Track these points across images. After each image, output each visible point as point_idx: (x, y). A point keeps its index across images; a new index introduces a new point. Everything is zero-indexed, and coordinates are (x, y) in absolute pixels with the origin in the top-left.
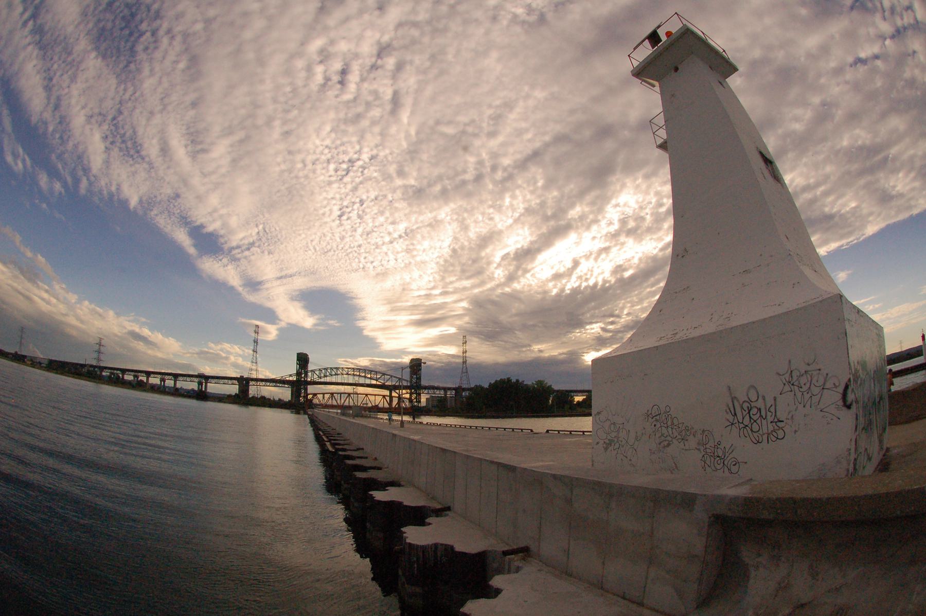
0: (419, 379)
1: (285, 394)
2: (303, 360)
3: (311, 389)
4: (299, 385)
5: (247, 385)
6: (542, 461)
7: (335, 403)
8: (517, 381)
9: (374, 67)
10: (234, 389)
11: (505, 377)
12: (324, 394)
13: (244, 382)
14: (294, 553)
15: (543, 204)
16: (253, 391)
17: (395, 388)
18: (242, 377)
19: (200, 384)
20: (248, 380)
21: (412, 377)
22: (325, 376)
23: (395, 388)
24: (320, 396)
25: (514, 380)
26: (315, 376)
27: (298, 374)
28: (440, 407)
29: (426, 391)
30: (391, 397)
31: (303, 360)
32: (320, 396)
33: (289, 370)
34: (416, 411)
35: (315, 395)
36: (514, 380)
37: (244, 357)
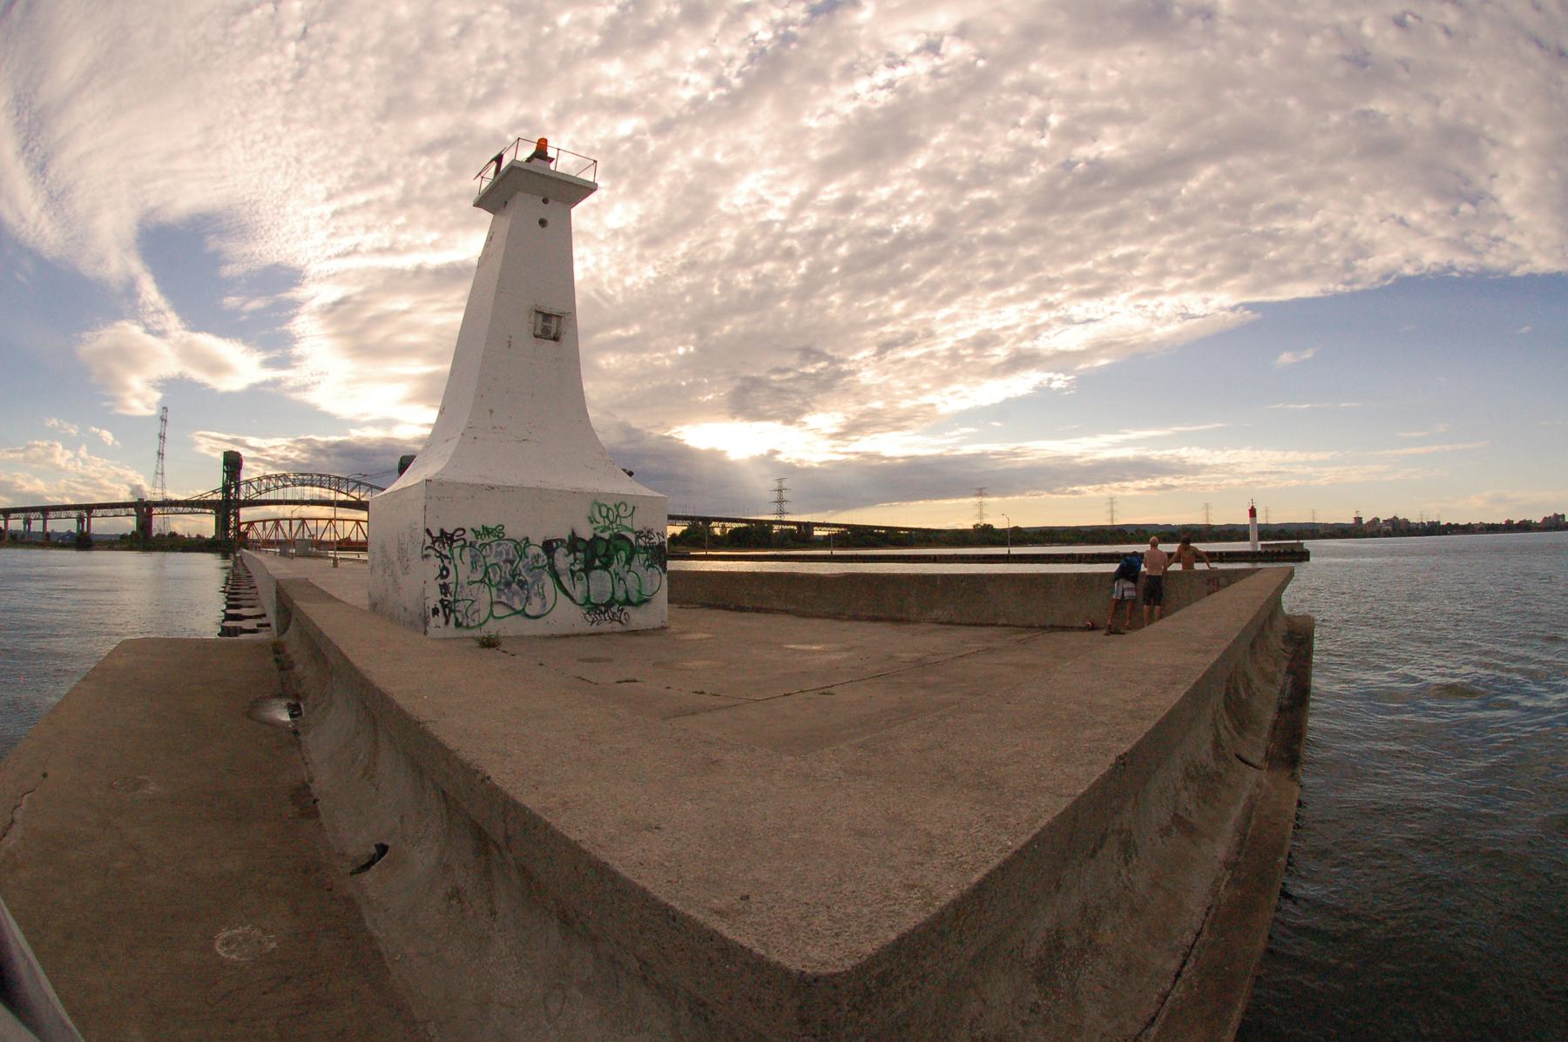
5: (150, 516)
24: (259, 526)
35: (251, 524)
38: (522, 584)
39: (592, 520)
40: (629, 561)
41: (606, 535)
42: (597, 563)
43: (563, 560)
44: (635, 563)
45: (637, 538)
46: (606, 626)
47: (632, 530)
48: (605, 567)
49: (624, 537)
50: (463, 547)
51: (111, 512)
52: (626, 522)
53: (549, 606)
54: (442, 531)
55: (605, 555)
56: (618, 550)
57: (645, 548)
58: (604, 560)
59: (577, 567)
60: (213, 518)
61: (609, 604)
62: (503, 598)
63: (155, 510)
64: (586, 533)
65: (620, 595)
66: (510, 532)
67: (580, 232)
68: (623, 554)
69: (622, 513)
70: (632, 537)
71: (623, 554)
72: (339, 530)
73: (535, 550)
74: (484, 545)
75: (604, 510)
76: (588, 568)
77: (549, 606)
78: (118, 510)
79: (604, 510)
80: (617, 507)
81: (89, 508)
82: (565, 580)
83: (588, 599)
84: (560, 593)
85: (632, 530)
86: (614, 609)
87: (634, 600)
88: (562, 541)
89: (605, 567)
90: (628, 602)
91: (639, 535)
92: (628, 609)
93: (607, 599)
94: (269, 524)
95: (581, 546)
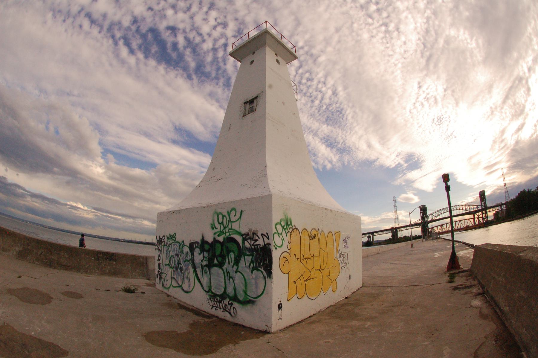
0: (485, 203)
1: (418, 231)
2: (423, 210)
3: (430, 225)
4: (424, 224)
5: (397, 232)
6: (102, 215)
7: (444, 231)
8: (528, 190)
9: (445, 95)
10: (388, 236)
11: (522, 190)
12: (437, 226)
13: (394, 231)
14: (101, 179)
15: (516, 111)
16: (401, 234)
17: (476, 212)
18: (393, 228)
19: (369, 237)
20: (396, 229)
21: (481, 203)
22: (439, 215)
23: (476, 212)
24: (435, 228)
25: (527, 190)
26: (433, 217)
27: (423, 218)
28: (498, 219)
29: (491, 209)
30: (474, 218)
31: (423, 210)
32: (435, 228)
33: (416, 218)
34: (487, 224)
35: (433, 228)
36: (527, 190)
37: (405, 216)
38: (181, 269)
39: (213, 227)
40: (237, 262)
41: (221, 239)
42: (216, 262)
43: (198, 257)
44: (242, 264)
45: (244, 240)
46: (220, 313)
47: (239, 233)
48: (221, 265)
49: (231, 240)
50: (164, 245)
51: (381, 233)
52: (235, 226)
53: (191, 289)
54: (170, 236)
55: (220, 255)
56: (229, 251)
57: (250, 250)
58: (220, 259)
59: (204, 263)
60: (420, 229)
61: (224, 296)
62: (175, 277)
63: (420, 234)
64: (209, 239)
65: (230, 291)
66: (179, 238)
67: (224, 109)
68: (232, 255)
69: (233, 219)
70: (239, 239)
71: (232, 255)
72: (463, 224)
73: (186, 249)
74: (170, 244)
75: (220, 216)
76: (210, 265)
77: (192, 285)
78: (379, 233)
79: (220, 216)
80: (229, 213)
81: (373, 233)
82: (199, 270)
83: (210, 289)
84: (196, 280)
85: (239, 233)
86: (226, 301)
87: (241, 298)
88: (197, 242)
89: (221, 265)
90: (235, 298)
91: (245, 237)
92: (236, 305)
93: (221, 292)
94: (439, 227)
95: (207, 247)
